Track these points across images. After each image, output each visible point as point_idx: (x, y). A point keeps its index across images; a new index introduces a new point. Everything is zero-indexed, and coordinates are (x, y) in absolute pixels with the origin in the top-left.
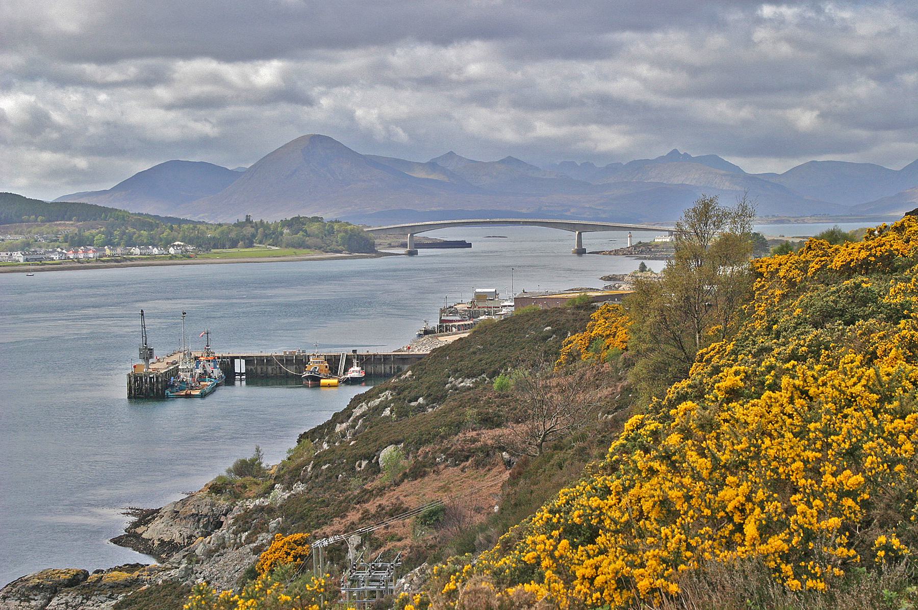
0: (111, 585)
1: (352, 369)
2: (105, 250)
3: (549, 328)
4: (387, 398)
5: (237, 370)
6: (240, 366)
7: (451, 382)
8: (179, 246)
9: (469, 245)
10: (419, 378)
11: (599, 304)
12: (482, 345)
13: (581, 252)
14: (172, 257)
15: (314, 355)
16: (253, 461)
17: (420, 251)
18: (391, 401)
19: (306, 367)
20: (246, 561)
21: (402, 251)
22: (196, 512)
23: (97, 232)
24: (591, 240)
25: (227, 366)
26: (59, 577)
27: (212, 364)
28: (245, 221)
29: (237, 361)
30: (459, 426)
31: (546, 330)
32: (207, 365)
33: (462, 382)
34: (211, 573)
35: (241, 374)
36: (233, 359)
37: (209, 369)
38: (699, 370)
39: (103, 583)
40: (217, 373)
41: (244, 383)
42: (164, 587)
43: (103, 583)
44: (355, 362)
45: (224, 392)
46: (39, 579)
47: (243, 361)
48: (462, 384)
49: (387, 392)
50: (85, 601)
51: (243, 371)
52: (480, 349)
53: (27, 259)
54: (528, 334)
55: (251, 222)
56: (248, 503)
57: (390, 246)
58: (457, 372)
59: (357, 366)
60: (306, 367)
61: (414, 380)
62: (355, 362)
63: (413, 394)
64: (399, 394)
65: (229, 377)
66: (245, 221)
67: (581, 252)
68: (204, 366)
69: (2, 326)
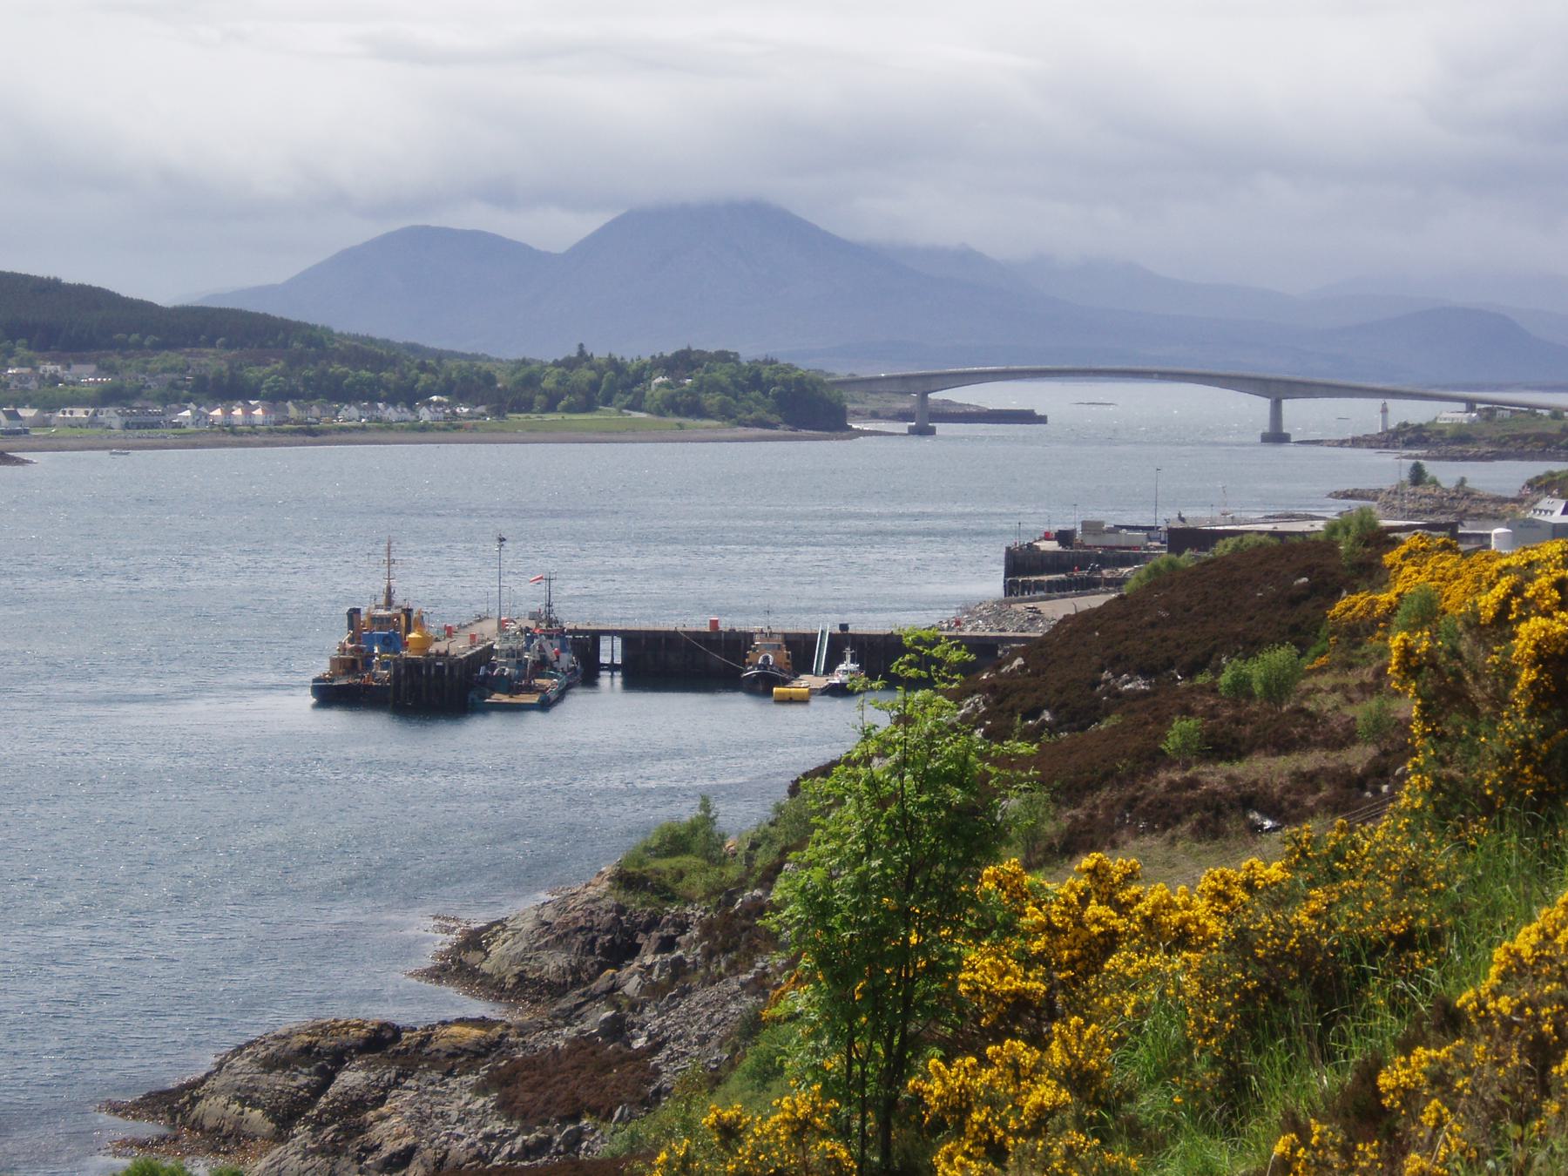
0: (450, 1051)
1: (842, 667)
2: (287, 410)
3: (1305, 580)
4: (976, 709)
5: (605, 659)
6: (610, 651)
7: (1107, 681)
8: (439, 404)
9: (1042, 420)
10: (1036, 674)
11: (1402, 535)
12: (1167, 609)
13: (1276, 436)
14: (424, 429)
15: (762, 632)
16: (693, 828)
17: (940, 428)
18: (985, 716)
19: (747, 656)
20: (733, 1007)
21: (903, 427)
22: (589, 924)
23: (268, 372)
24: (1300, 413)
25: (585, 646)
26: (347, 1033)
27: (557, 642)
28: (1284, 401)
29: (605, 644)
30: (1155, 758)
31: (1299, 585)
32: (546, 645)
33: (1127, 682)
34: (662, 1028)
35: (612, 667)
36: (596, 635)
37: (551, 653)
38: (1048, 1095)
39: (434, 1047)
40: (567, 660)
41: (618, 680)
42: (571, 1052)
43: (434, 1047)
44: (848, 652)
45: (578, 701)
46: (309, 1034)
47: (618, 642)
48: (1129, 686)
49: (976, 698)
50: (401, 1080)
51: (618, 660)
52: (1163, 619)
53: (127, 423)
54: (1261, 590)
55: (590, 359)
56: (689, 910)
57: (875, 416)
58: (1118, 663)
59: (852, 662)
60: (747, 656)
61: (1029, 675)
62: (848, 652)
63: (1030, 702)
64: (998, 702)
65: (588, 673)
66: (1284, 401)
67: (1276, 436)
68: (540, 646)
69: (1557, 467)
